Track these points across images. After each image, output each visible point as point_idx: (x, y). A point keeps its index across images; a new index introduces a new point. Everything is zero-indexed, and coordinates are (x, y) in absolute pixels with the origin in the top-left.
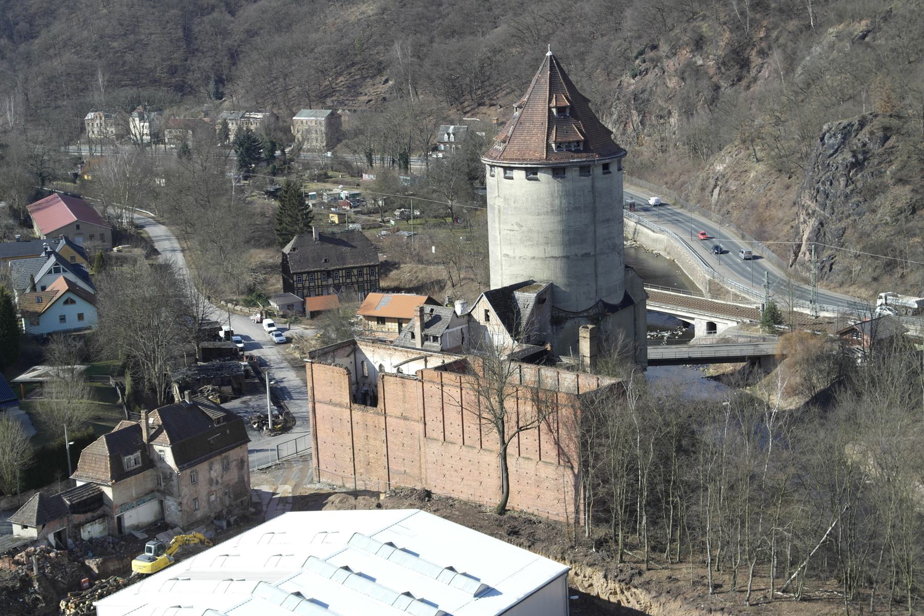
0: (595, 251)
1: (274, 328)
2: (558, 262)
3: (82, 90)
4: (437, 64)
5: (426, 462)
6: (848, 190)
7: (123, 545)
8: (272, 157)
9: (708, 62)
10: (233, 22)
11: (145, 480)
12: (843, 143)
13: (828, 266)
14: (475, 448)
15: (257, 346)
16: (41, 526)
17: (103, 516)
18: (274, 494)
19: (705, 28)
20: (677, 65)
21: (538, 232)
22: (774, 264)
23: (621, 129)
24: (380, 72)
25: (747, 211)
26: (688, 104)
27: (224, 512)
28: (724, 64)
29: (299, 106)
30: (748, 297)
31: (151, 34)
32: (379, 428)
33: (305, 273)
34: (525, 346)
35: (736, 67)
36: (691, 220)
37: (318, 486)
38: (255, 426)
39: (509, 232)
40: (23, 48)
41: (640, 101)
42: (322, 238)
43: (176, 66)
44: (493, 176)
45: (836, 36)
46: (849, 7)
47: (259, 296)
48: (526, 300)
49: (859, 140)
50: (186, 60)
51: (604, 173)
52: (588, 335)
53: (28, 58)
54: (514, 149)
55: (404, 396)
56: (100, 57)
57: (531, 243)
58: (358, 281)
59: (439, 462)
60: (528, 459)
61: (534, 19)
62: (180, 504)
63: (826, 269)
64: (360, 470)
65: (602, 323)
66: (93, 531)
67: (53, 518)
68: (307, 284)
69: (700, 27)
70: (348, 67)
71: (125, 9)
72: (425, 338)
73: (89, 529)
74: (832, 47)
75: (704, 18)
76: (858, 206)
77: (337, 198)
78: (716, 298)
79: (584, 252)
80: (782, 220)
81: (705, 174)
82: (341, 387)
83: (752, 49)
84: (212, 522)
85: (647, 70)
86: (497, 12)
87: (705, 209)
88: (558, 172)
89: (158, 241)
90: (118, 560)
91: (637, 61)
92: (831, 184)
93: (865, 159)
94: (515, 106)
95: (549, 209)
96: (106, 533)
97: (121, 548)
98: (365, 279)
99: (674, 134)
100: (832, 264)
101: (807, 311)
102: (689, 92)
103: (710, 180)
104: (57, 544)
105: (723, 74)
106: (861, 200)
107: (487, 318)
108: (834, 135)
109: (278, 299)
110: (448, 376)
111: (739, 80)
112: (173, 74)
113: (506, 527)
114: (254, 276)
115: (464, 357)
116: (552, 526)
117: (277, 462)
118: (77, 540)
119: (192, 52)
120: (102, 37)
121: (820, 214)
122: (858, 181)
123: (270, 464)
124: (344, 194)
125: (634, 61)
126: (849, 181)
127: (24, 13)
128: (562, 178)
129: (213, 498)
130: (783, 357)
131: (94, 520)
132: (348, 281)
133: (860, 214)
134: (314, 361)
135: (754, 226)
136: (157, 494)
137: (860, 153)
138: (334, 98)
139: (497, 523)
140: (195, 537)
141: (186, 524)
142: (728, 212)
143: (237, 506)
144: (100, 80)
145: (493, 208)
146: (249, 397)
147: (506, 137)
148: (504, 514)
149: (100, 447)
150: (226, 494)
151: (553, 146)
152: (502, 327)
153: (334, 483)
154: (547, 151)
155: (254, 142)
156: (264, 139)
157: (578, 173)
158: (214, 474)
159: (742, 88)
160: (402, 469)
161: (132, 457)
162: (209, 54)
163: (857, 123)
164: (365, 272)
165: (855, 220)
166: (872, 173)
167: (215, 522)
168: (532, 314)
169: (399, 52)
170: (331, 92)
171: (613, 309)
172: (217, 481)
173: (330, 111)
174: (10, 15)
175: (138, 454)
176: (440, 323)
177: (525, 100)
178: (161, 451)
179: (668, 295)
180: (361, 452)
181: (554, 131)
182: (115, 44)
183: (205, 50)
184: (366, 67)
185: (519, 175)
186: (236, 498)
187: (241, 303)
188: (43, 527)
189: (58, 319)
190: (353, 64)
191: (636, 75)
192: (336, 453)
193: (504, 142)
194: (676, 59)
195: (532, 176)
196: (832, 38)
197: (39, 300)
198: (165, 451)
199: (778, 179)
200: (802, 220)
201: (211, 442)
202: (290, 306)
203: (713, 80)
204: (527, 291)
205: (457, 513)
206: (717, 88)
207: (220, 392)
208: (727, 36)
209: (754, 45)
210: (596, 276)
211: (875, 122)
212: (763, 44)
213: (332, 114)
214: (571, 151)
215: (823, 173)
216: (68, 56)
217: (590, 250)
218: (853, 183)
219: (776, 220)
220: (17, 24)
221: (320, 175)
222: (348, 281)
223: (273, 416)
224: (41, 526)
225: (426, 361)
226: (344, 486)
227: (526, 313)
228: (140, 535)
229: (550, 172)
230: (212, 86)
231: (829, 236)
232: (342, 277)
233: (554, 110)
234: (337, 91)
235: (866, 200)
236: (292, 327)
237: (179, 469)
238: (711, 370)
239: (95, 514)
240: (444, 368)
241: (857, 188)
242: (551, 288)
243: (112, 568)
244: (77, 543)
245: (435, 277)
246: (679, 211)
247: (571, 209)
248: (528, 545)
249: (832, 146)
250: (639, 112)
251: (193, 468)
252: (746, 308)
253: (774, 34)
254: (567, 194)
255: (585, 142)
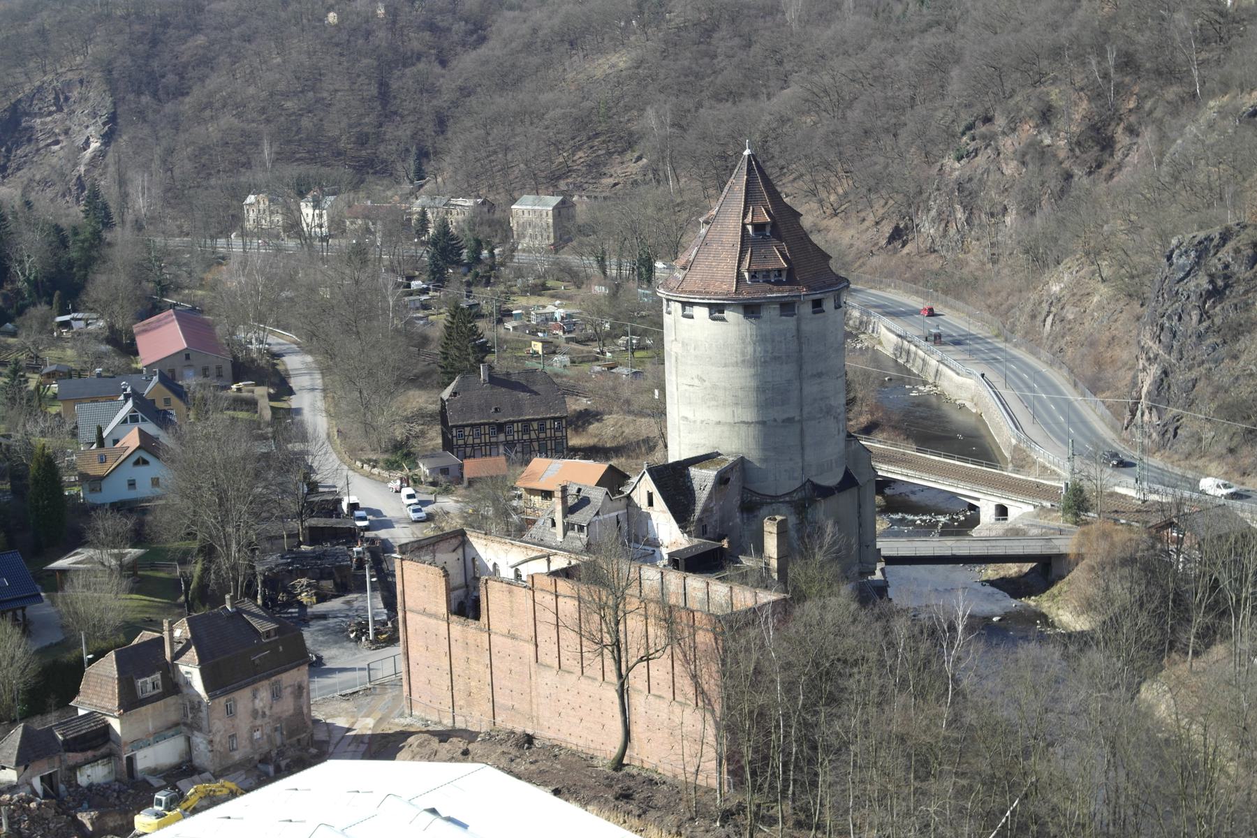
0: (801, 415)
1: (415, 501)
2: (751, 428)
3: (243, 165)
4: (703, 137)
5: (538, 695)
6: (1202, 328)
7: (131, 794)
8: (477, 259)
9: (1057, 141)
10: (443, 76)
11: (167, 710)
12: (1197, 263)
13: (1171, 430)
14: (595, 679)
15: (388, 524)
16: (22, 768)
17: (109, 756)
18: (349, 730)
19: (1055, 95)
20: (1016, 145)
21: (725, 389)
22: (1107, 425)
23: (941, 229)
24: (630, 145)
25: (1084, 350)
26: (1030, 198)
27: (274, 753)
28: (1079, 144)
29: (523, 189)
30: (1059, 471)
31: (336, 91)
32: (482, 648)
33: (467, 426)
34: (696, 541)
35: (1096, 148)
36: (1014, 359)
37: (408, 720)
38: (352, 636)
39: (688, 388)
40: (169, 108)
41: (966, 193)
42: (494, 380)
43: (367, 135)
44: (669, 313)
45: (1219, 112)
46: (1238, 73)
47: (407, 455)
48: (703, 479)
49: (1220, 260)
50: (381, 125)
51: (814, 313)
52: (775, 530)
53: (176, 123)
54: (695, 279)
55: (511, 607)
56: (268, 121)
57: (715, 403)
58: (538, 437)
59: (554, 697)
60: (660, 697)
61: (834, 79)
62: (211, 742)
63: (1170, 435)
64: (459, 702)
65: (809, 510)
66: (94, 774)
67: (39, 757)
68: (470, 441)
69: (1048, 93)
70: (589, 139)
71: (304, 58)
72: (568, 527)
73: (89, 772)
74: (1211, 126)
75: (1055, 80)
76: (1214, 349)
77: (549, 318)
78: (1018, 472)
79: (786, 416)
80: (1126, 364)
81: (1037, 297)
82: (437, 593)
83: (1118, 124)
84: (256, 766)
85: (976, 151)
86: (788, 66)
87: (1032, 341)
88: (750, 310)
89: (297, 375)
90: (120, 814)
91: (965, 139)
92: (1180, 319)
93: (1227, 286)
94: (701, 220)
95: (740, 359)
96: (112, 778)
97: (127, 799)
98: (549, 435)
99: (1011, 237)
100: (1177, 428)
101: (1132, 493)
102: (1030, 182)
103: (1044, 305)
104: (45, 790)
105: (1077, 157)
106: (1219, 341)
107: (651, 503)
108: (1186, 252)
109: (427, 460)
110: (564, 586)
111: (1099, 166)
112: (363, 144)
113: (616, 788)
114: (408, 427)
115: (594, 557)
116: (677, 790)
117: (368, 686)
118: (71, 786)
119: (388, 115)
120: (271, 95)
121: (1165, 360)
122: (1216, 315)
123: (357, 689)
124: (559, 313)
125: (960, 138)
126: (1204, 315)
127: (174, 61)
128: (755, 318)
129: (257, 735)
130: (1080, 557)
131: (96, 761)
132: (526, 437)
133: (1217, 362)
134: (404, 557)
135: (1089, 371)
136: (184, 729)
137: (1219, 277)
138: (570, 180)
139: (607, 781)
140: (223, 786)
141: (218, 769)
142: (1061, 350)
143: (292, 745)
144: (266, 153)
145: (670, 355)
146: (356, 595)
147: (688, 261)
148: (621, 770)
149: (108, 666)
150: (276, 729)
151: (746, 275)
152: (669, 515)
153: (427, 718)
154: (737, 282)
155: (453, 240)
156: (467, 238)
157: (777, 312)
158: (259, 704)
159: (1103, 177)
160: (510, 704)
161: (149, 680)
162: (410, 118)
163: (1218, 237)
164: (548, 426)
165: (1210, 369)
166: (1236, 305)
167: (259, 766)
168: (710, 497)
169: (652, 120)
170: (566, 172)
171: (826, 492)
172: (264, 714)
173: (560, 198)
174: (155, 64)
175: (158, 676)
176: (588, 507)
177: (714, 213)
178: (187, 673)
179: (951, 464)
180: (461, 679)
181: (748, 256)
182: (289, 104)
183: (406, 113)
184: (614, 139)
185: (701, 313)
186: (291, 735)
187: (381, 464)
188: (26, 769)
189: (126, 484)
190: (597, 135)
191: (962, 157)
192: (431, 678)
193: (684, 268)
194: (1014, 137)
195: (717, 314)
196: (1212, 114)
197: (103, 460)
198: (191, 671)
199: (1127, 307)
200: (1141, 367)
201: (257, 662)
202: (445, 471)
203: (1063, 165)
204: (706, 468)
205: (559, 766)
206: (1068, 176)
207: (317, 587)
208: (1084, 106)
209: (1121, 119)
210: (803, 448)
211: (1243, 235)
212: (1133, 119)
213: (563, 202)
214: (769, 282)
215: (1169, 303)
216: (228, 120)
217: (794, 413)
218: (1209, 318)
219: (1119, 364)
220: (163, 76)
221: (536, 285)
222: (526, 437)
223: (375, 622)
224: (22, 768)
225: (549, 561)
226: (440, 722)
227: (702, 496)
228: (155, 781)
229: (741, 310)
230: (411, 163)
231: (1174, 389)
232: (518, 432)
233: (750, 228)
234: (574, 171)
235: (1225, 342)
236: (440, 499)
237: (210, 697)
238: (989, 572)
239: (98, 753)
240: (566, 573)
241: (1213, 325)
242: (742, 463)
243: (111, 824)
244: (71, 790)
245: (644, 433)
246: (1001, 345)
247: (768, 359)
248: (637, 813)
249: (1182, 268)
250: (965, 208)
251: (230, 696)
252: (1051, 486)
253: (1148, 105)
254: (762, 339)
255: (790, 271)
